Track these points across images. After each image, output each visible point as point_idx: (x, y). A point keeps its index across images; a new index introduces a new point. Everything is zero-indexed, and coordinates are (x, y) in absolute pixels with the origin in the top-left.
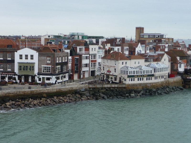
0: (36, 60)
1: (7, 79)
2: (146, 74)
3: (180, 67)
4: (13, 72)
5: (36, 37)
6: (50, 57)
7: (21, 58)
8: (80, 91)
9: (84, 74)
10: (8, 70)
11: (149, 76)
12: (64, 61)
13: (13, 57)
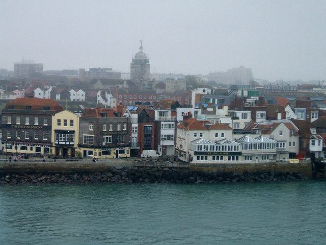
0: (75, 128)
1: (42, 152)
2: (227, 151)
3: (313, 144)
4: (49, 142)
5: (279, 87)
6: (93, 123)
7: (59, 124)
8: (115, 168)
9: (165, 150)
10: (44, 139)
11: (232, 153)
12: (119, 129)
13: (50, 122)
